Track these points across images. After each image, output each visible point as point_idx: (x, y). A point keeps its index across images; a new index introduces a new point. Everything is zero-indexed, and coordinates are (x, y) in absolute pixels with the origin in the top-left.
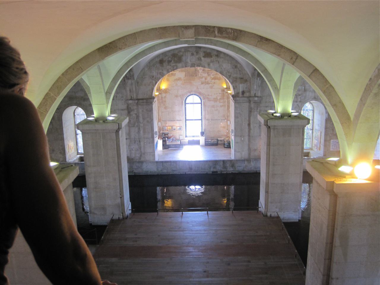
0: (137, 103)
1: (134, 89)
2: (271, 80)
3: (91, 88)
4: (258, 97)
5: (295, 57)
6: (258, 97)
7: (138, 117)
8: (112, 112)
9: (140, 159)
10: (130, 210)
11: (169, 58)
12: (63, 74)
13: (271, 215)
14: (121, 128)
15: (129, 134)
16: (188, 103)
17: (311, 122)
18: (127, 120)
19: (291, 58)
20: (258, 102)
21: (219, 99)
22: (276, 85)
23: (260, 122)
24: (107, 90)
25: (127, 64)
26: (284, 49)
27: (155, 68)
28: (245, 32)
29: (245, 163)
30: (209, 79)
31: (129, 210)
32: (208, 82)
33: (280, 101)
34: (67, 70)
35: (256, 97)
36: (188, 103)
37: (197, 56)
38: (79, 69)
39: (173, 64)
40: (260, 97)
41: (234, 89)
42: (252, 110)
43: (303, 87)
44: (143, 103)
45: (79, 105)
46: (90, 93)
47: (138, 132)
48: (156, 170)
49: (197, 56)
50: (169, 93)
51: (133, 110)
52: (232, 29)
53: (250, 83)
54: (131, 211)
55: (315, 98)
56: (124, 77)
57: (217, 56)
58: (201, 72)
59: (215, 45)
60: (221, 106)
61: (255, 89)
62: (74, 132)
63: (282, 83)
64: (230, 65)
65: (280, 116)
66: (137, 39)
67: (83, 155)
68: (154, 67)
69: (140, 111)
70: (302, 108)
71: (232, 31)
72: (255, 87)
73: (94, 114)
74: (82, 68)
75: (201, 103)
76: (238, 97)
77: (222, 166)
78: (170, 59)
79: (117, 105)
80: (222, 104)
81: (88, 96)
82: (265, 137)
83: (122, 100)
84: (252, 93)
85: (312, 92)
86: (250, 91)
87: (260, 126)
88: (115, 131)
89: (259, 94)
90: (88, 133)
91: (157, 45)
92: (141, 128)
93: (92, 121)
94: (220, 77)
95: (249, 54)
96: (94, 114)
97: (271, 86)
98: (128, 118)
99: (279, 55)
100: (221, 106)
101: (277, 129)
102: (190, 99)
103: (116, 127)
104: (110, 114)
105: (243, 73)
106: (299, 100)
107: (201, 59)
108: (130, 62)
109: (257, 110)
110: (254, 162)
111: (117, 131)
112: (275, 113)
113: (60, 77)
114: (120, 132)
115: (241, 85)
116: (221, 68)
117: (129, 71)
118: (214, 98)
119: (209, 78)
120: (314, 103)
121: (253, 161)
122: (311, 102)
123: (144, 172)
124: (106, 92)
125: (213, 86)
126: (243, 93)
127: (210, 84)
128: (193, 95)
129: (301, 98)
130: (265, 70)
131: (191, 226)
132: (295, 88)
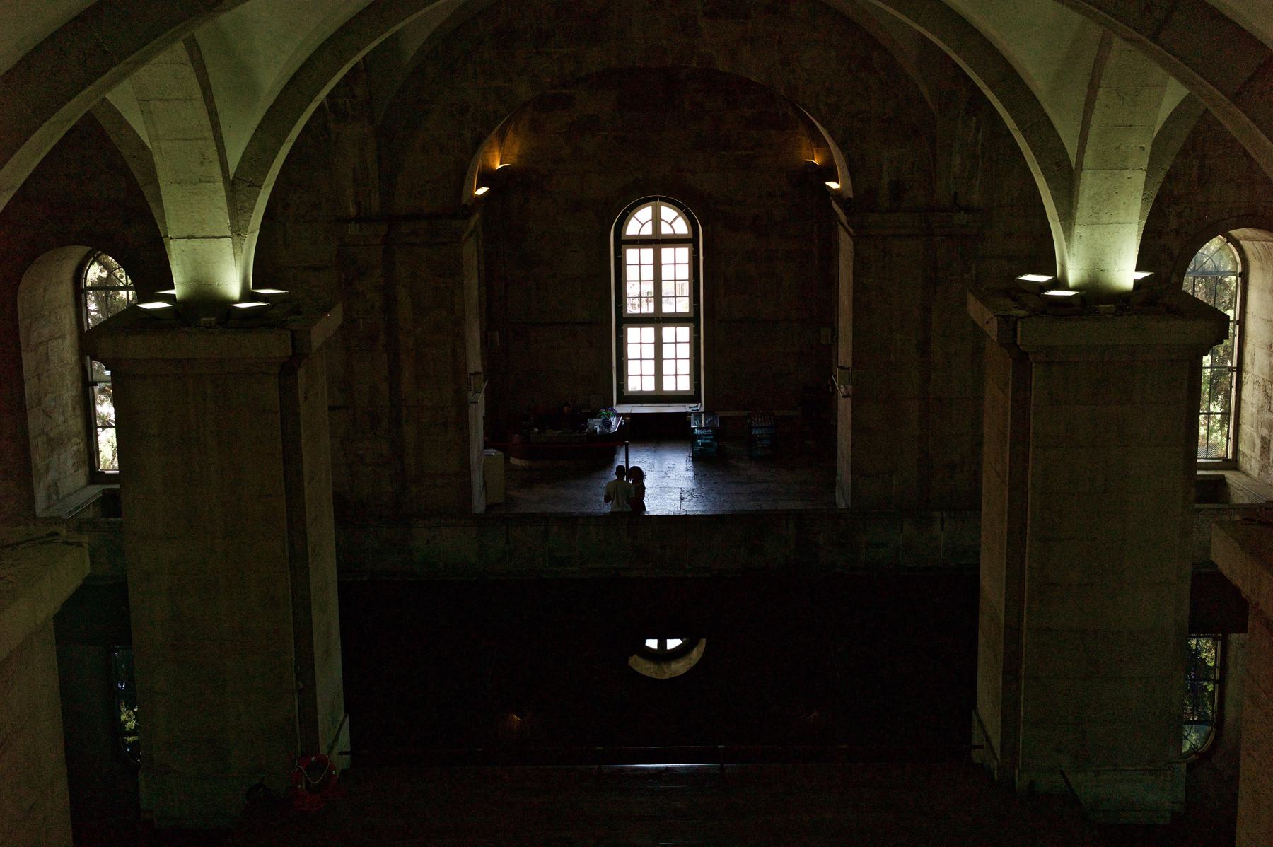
2: (1040, 129)
3: (157, 158)
4: (968, 210)
6: (968, 210)
8: (263, 271)
10: (193, 48)
13: (1032, 783)
17: (1234, 329)
18: (334, 318)
22: (1063, 150)
23: (978, 332)
31: (341, 753)
33: (1078, 229)
41: (853, 171)
45: (97, 247)
46: (155, 182)
54: (348, 757)
63: (1092, 139)
67: (117, 486)
70: (1187, 267)
73: (172, 287)
96: (172, 287)
98: (339, 309)
102: (640, 223)
103: (276, 346)
110: (946, 525)
111: (288, 369)
114: (301, 373)
120: (1246, 239)
121: (942, 518)
122: (1235, 233)
124: (234, 177)
126: (898, 190)
131: (655, 790)
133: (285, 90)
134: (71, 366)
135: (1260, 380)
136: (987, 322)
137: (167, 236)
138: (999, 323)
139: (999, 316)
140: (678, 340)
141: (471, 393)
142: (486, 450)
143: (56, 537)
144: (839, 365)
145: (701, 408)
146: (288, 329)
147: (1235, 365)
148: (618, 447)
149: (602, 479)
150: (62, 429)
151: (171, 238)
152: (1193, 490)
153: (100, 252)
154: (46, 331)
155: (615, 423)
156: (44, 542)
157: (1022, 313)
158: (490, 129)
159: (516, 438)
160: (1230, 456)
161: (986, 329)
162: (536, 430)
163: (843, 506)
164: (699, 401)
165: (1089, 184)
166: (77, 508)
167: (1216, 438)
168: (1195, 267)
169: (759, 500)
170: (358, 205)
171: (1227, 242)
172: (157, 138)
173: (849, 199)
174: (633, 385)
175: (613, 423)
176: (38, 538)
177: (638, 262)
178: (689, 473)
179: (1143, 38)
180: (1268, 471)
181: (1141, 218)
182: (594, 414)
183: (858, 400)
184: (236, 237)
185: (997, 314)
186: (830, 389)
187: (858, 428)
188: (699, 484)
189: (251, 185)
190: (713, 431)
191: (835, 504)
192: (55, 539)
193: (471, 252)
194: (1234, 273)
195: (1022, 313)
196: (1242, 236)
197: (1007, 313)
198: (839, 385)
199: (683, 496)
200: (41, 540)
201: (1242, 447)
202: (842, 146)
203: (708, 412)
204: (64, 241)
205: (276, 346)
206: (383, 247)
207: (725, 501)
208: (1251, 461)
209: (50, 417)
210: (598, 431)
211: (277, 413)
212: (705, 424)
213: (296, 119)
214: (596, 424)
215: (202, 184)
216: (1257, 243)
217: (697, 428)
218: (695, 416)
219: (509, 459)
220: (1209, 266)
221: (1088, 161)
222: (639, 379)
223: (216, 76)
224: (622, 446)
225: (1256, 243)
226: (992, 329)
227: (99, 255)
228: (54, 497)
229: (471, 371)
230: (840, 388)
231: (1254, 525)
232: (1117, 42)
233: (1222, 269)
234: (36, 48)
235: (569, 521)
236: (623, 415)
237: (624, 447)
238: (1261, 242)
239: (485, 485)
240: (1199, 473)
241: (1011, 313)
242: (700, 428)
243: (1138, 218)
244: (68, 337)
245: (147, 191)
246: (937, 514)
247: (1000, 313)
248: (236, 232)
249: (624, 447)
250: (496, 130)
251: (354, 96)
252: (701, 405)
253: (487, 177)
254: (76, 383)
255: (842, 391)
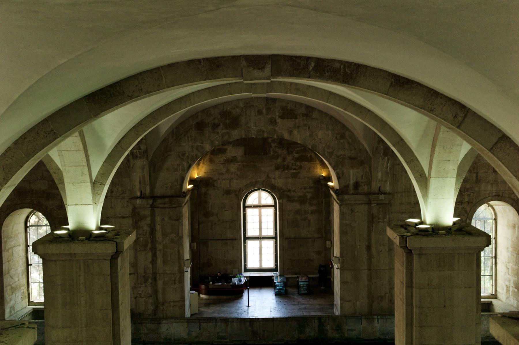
0: (152, 204)
1: (147, 178)
2: (413, 161)
3: (64, 174)
4: (385, 194)
5: (462, 114)
6: (385, 194)
7: (153, 231)
8: (104, 220)
9: (155, 315)
11: (214, 119)
12: (16, 143)
14: (122, 252)
15: (134, 265)
16: (267, 197)
17: (493, 241)
18: (133, 237)
19: (454, 115)
20: (386, 204)
21: (309, 197)
22: (423, 170)
24: (97, 177)
25: (136, 129)
26: (441, 98)
27: (188, 138)
28: (366, 67)
29: (361, 324)
30: (289, 158)
32: (288, 166)
33: (430, 201)
34: (25, 134)
35: (382, 193)
36: (267, 197)
37: (269, 116)
38: (49, 134)
39: (222, 130)
40: (389, 194)
41: (339, 178)
42: (374, 220)
43: (475, 175)
44: (165, 203)
45: (37, 207)
46: (63, 183)
47: (153, 260)
48: (185, 336)
49: (269, 116)
50: (214, 186)
51: (144, 217)
52: (339, 61)
53: (370, 167)
55: (499, 196)
56: (128, 155)
57: (306, 115)
58: (275, 147)
59: (305, 94)
60: (313, 212)
61: (380, 177)
62: (25, 260)
64: (330, 132)
65: (430, 230)
66: (162, 79)
68: (186, 137)
69: (158, 219)
71: (342, 66)
72: (380, 174)
73: (68, 225)
74: (55, 131)
75: (275, 206)
76: (347, 193)
77: (317, 329)
78: (216, 121)
79: (112, 208)
80: (314, 208)
81: (58, 189)
82: (403, 272)
83: (123, 198)
84: (375, 186)
85: (492, 184)
86: (369, 183)
87: (391, 250)
88: (110, 258)
89: (388, 188)
90: (55, 261)
91: (193, 93)
92: (158, 253)
93: (62, 236)
94: (311, 156)
95: (369, 111)
96: (68, 225)
97: (413, 173)
98: (134, 234)
99: (431, 111)
100: (313, 212)
101: (425, 254)
102: (253, 198)
103: (109, 248)
104: (101, 225)
105: (355, 149)
106: (467, 199)
107: (275, 120)
108: (141, 125)
109: (384, 219)
110: (379, 321)
111: (114, 258)
112: (422, 223)
113: (9, 147)
114: (119, 260)
115: (351, 172)
116: (314, 139)
117: (138, 144)
118: (300, 197)
119: (289, 158)
120: (496, 205)
121: (378, 319)
122: (491, 203)
123: (162, 340)
124: (95, 181)
125: (299, 172)
126: (357, 185)
127: (291, 169)
128: (259, 190)
129: (469, 196)
130: (400, 142)
132: (458, 174)
133: (116, 147)
134: (22, 258)
135: (504, 262)
136: (395, 238)
137: (67, 204)
138: (400, 238)
139: (399, 235)
140: (269, 246)
141: (185, 268)
142: (191, 291)
143: (24, 325)
144: (334, 256)
145: (278, 273)
146: (115, 241)
147: (494, 255)
148: (244, 290)
149: (238, 303)
150: (17, 283)
151: (68, 205)
152: (480, 306)
153: (36, 211)
154: (12, 243)
155: (243, 280)
156: (19, 327)
157: (409, 234)
158: (194, 162)
159: (203, 287)
160: (494, 293)
161: (395, 240)
162: (211, 283)
163: (337, 314)
164: (277, 271)
165: (433, 183)
166: (22, 316)
167: (487, 286)
168: (476, 216)
169: (303, 312)
170: (141, 192)
171: (488, 206)
172: (65, 166)
173: (337, 189)
174: (250, 266)
175: (242, 280)
176: (17, 326)
177: (252, 215)
178: (274, 300)
179: (454, 127)
180: (509, 299)
181: (454, 197)
182: (235, 277)
183: (342, 269)
184: (94, 205)
185: (399, 235)
186: (331, 266)
187: (343, 282)
188: (278, 305)
189: (101, 184)
190: (283, 283)
191: (333, 313)
192: (24, 326)
193: (186, 211)
194: (492, 219)
195: (409, 234)
196: (494, 204)
197: (402, 235)
198: (335, 264)
199: (272, 310)
200: (18, 327)
201: (498, 289)
202: (334, 168)
203: (281, 275)
204: (22, 207)
205: (109, 248)
206: (151, 209)
207: (289, 312)
208: (502, 294)
209: (13, 278)
210: (236, 283)
211: (109, 275)
212: (280, 281)
213: (186, 165)
214: (235, 281)
215: (82, 184)
216: (500, 207)
217: (277, 282)
218: (276, 277)
219: (200, 295)
220: (481, 216)
221: (433, 174)
222: (252, 262)
223: (89, 141)
224: (246, 289)
225: (500, 207)
226: (397, 241)
227: (35, 212)
228: (13, 312)
229: (185, 259)
230: (335, 265)
231: (506, 318)
232: (443, 128)
233: (486, 217)
234: (28, 131)
235: (225, 320)
236: (247, 277)
237: (247, 290)
238: (502, 207)
239: (190, 305)
240: (482, 300)
241: (404, 234)
242: (278, 282)
243: (453, 197)
244: (21, 245)
245: (59, 186)
246: (376, 317)
247: (400, 234)
248: (94, 203)
249: (247, 290)
250: (196, 163)
251: (140, 149)
252: (278, 273)
253: (192, 181)
254: (24, 264)
255: (336, 267)
